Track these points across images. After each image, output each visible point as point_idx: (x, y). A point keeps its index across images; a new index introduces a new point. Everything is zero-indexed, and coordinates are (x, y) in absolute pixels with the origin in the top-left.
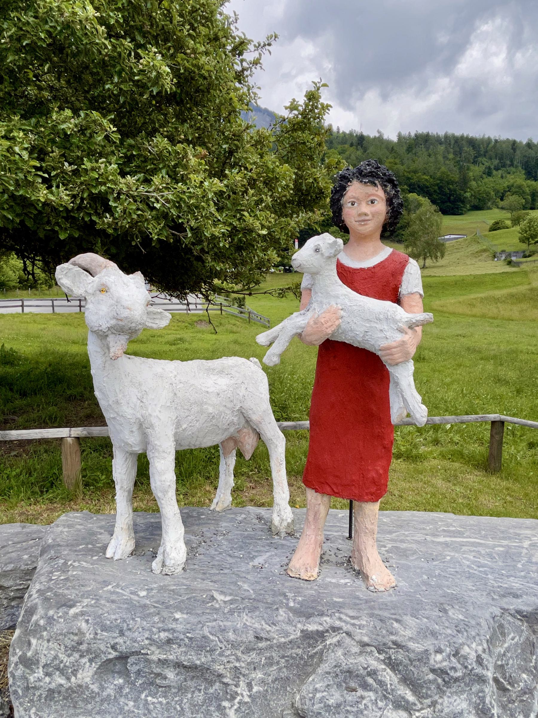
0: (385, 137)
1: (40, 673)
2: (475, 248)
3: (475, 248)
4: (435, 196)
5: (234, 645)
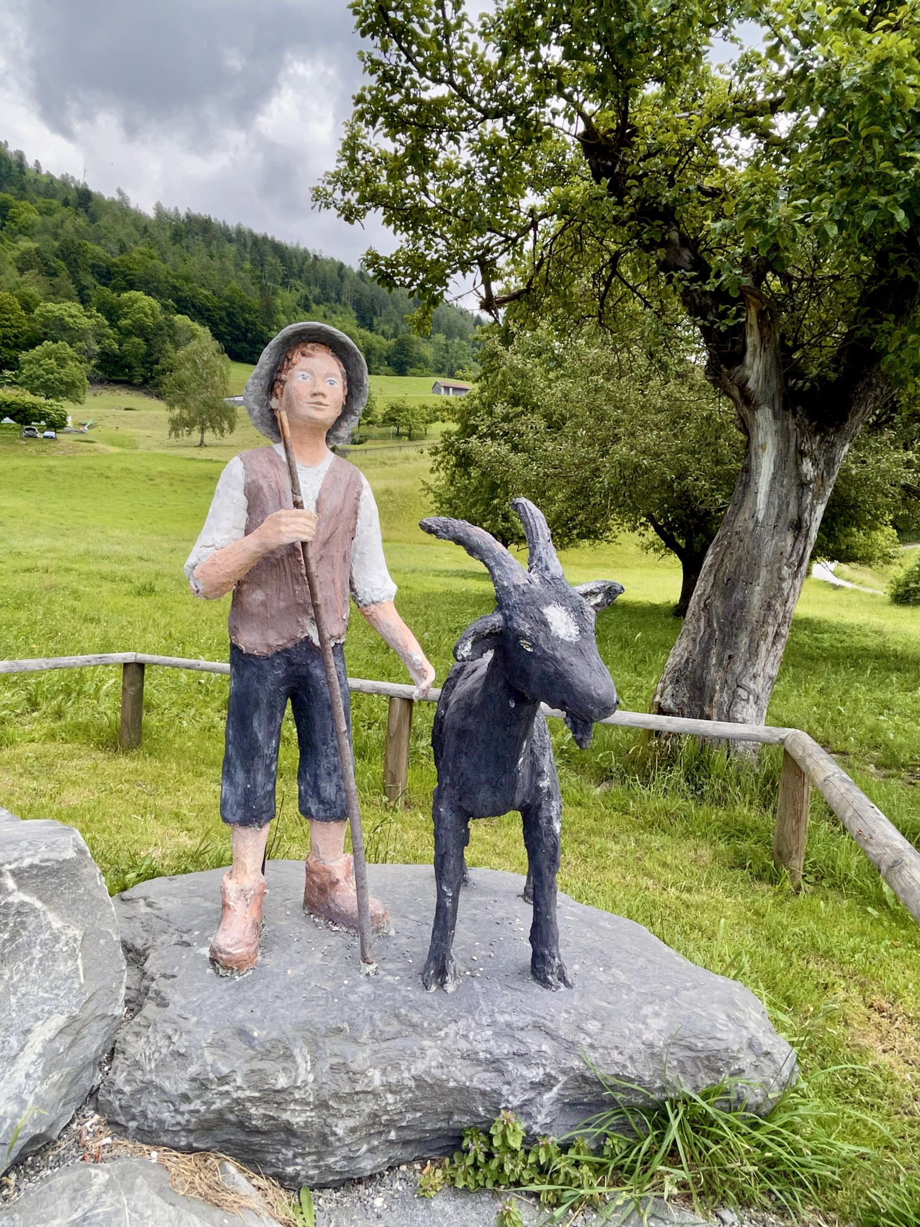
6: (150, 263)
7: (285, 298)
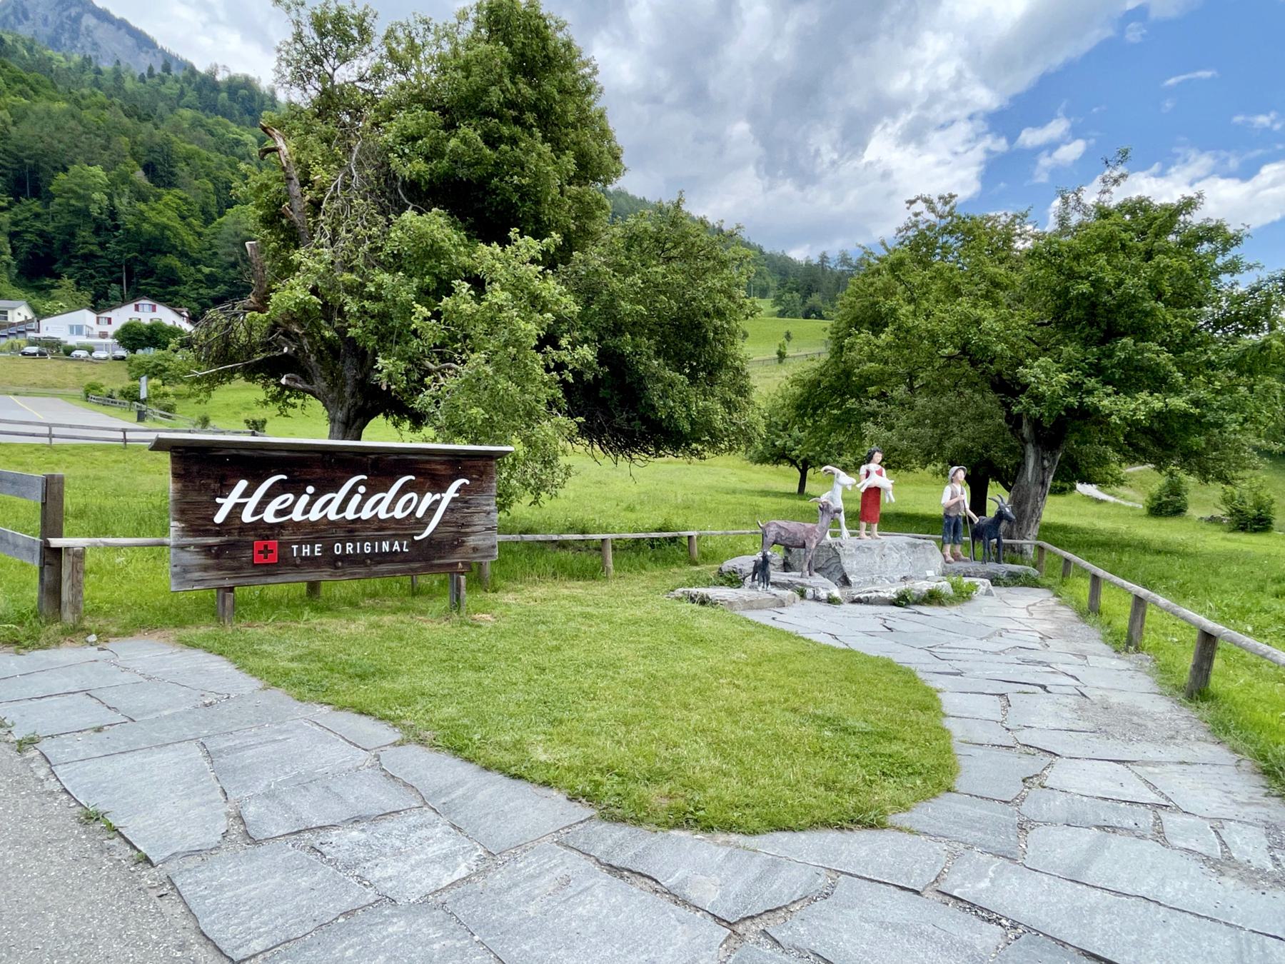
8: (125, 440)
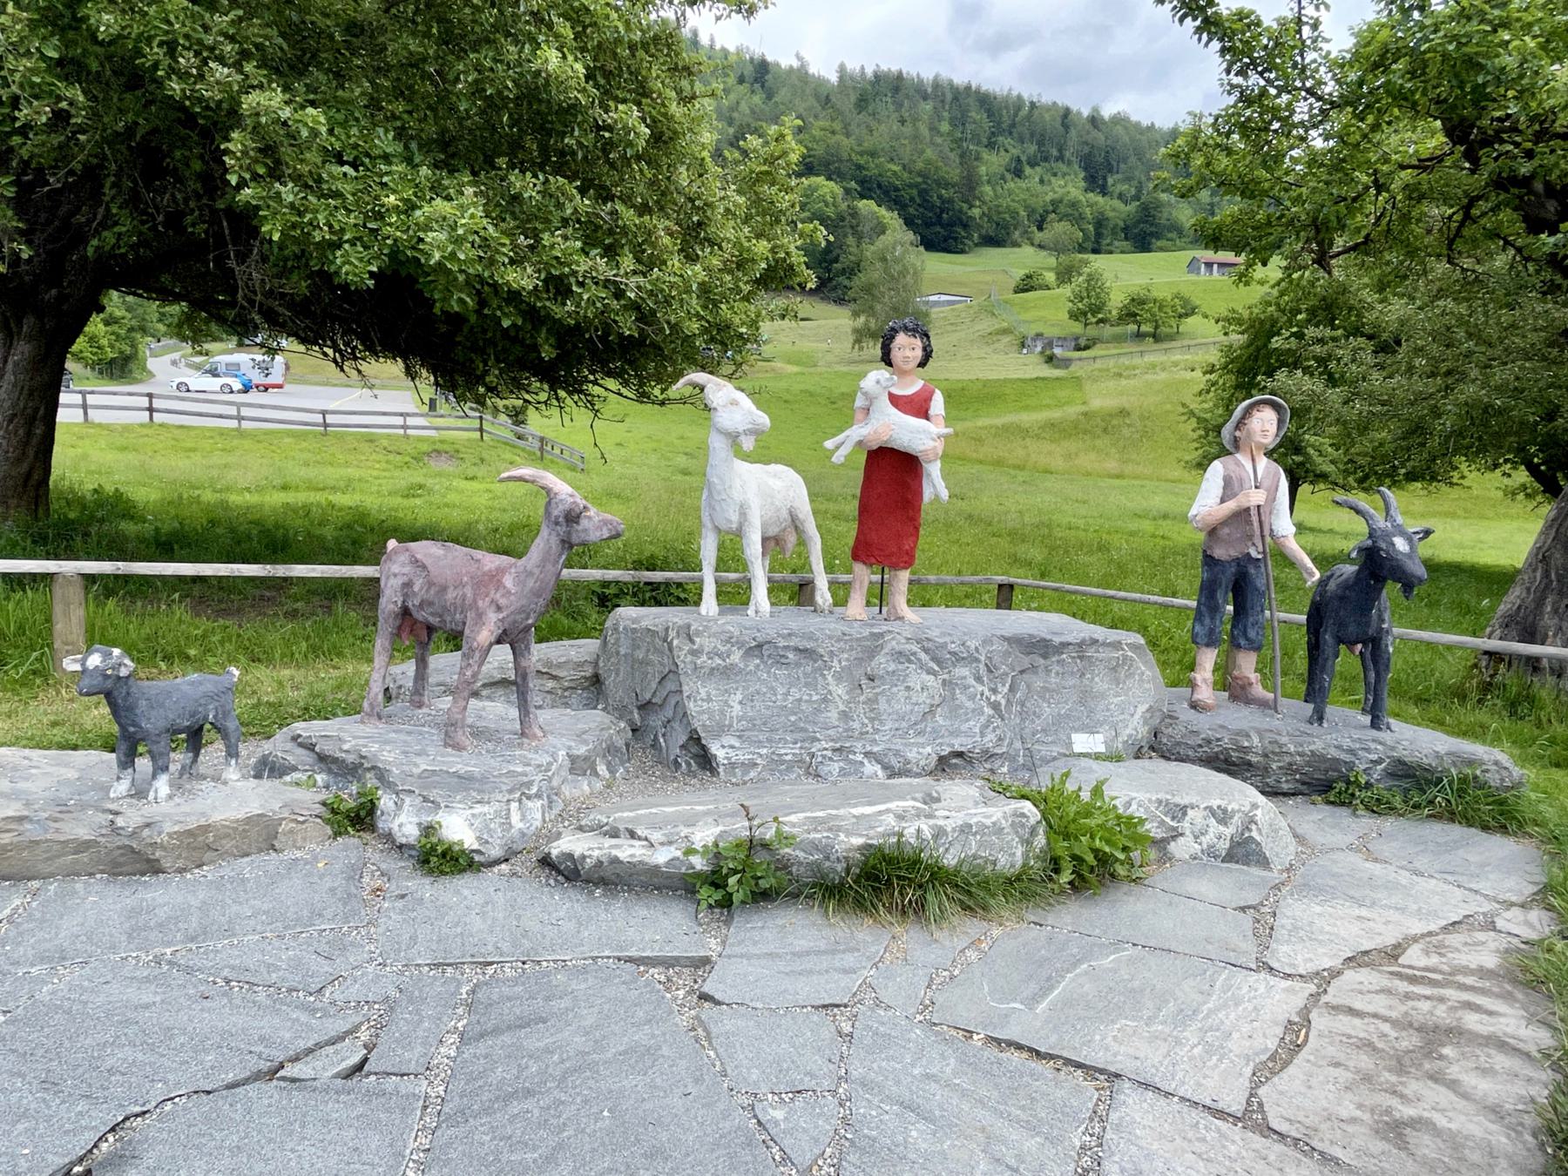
0: (813, 70)
1: (704, 658)
2: (986, 325)
3: (986, 325)
4: (911, 210)
5: (830, 637)
6: (833, 140)
7: (992, 163)
8: (326, 425)
